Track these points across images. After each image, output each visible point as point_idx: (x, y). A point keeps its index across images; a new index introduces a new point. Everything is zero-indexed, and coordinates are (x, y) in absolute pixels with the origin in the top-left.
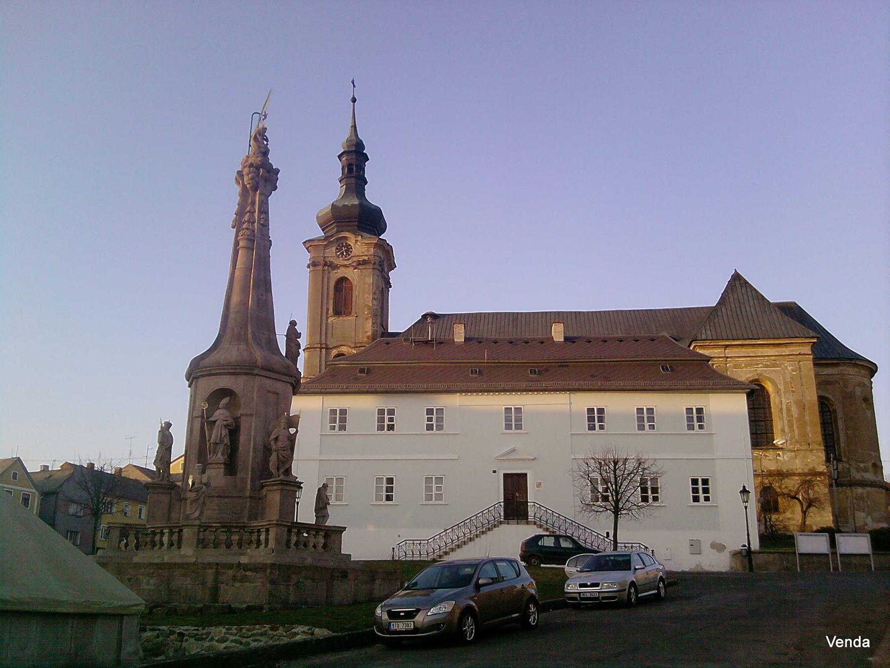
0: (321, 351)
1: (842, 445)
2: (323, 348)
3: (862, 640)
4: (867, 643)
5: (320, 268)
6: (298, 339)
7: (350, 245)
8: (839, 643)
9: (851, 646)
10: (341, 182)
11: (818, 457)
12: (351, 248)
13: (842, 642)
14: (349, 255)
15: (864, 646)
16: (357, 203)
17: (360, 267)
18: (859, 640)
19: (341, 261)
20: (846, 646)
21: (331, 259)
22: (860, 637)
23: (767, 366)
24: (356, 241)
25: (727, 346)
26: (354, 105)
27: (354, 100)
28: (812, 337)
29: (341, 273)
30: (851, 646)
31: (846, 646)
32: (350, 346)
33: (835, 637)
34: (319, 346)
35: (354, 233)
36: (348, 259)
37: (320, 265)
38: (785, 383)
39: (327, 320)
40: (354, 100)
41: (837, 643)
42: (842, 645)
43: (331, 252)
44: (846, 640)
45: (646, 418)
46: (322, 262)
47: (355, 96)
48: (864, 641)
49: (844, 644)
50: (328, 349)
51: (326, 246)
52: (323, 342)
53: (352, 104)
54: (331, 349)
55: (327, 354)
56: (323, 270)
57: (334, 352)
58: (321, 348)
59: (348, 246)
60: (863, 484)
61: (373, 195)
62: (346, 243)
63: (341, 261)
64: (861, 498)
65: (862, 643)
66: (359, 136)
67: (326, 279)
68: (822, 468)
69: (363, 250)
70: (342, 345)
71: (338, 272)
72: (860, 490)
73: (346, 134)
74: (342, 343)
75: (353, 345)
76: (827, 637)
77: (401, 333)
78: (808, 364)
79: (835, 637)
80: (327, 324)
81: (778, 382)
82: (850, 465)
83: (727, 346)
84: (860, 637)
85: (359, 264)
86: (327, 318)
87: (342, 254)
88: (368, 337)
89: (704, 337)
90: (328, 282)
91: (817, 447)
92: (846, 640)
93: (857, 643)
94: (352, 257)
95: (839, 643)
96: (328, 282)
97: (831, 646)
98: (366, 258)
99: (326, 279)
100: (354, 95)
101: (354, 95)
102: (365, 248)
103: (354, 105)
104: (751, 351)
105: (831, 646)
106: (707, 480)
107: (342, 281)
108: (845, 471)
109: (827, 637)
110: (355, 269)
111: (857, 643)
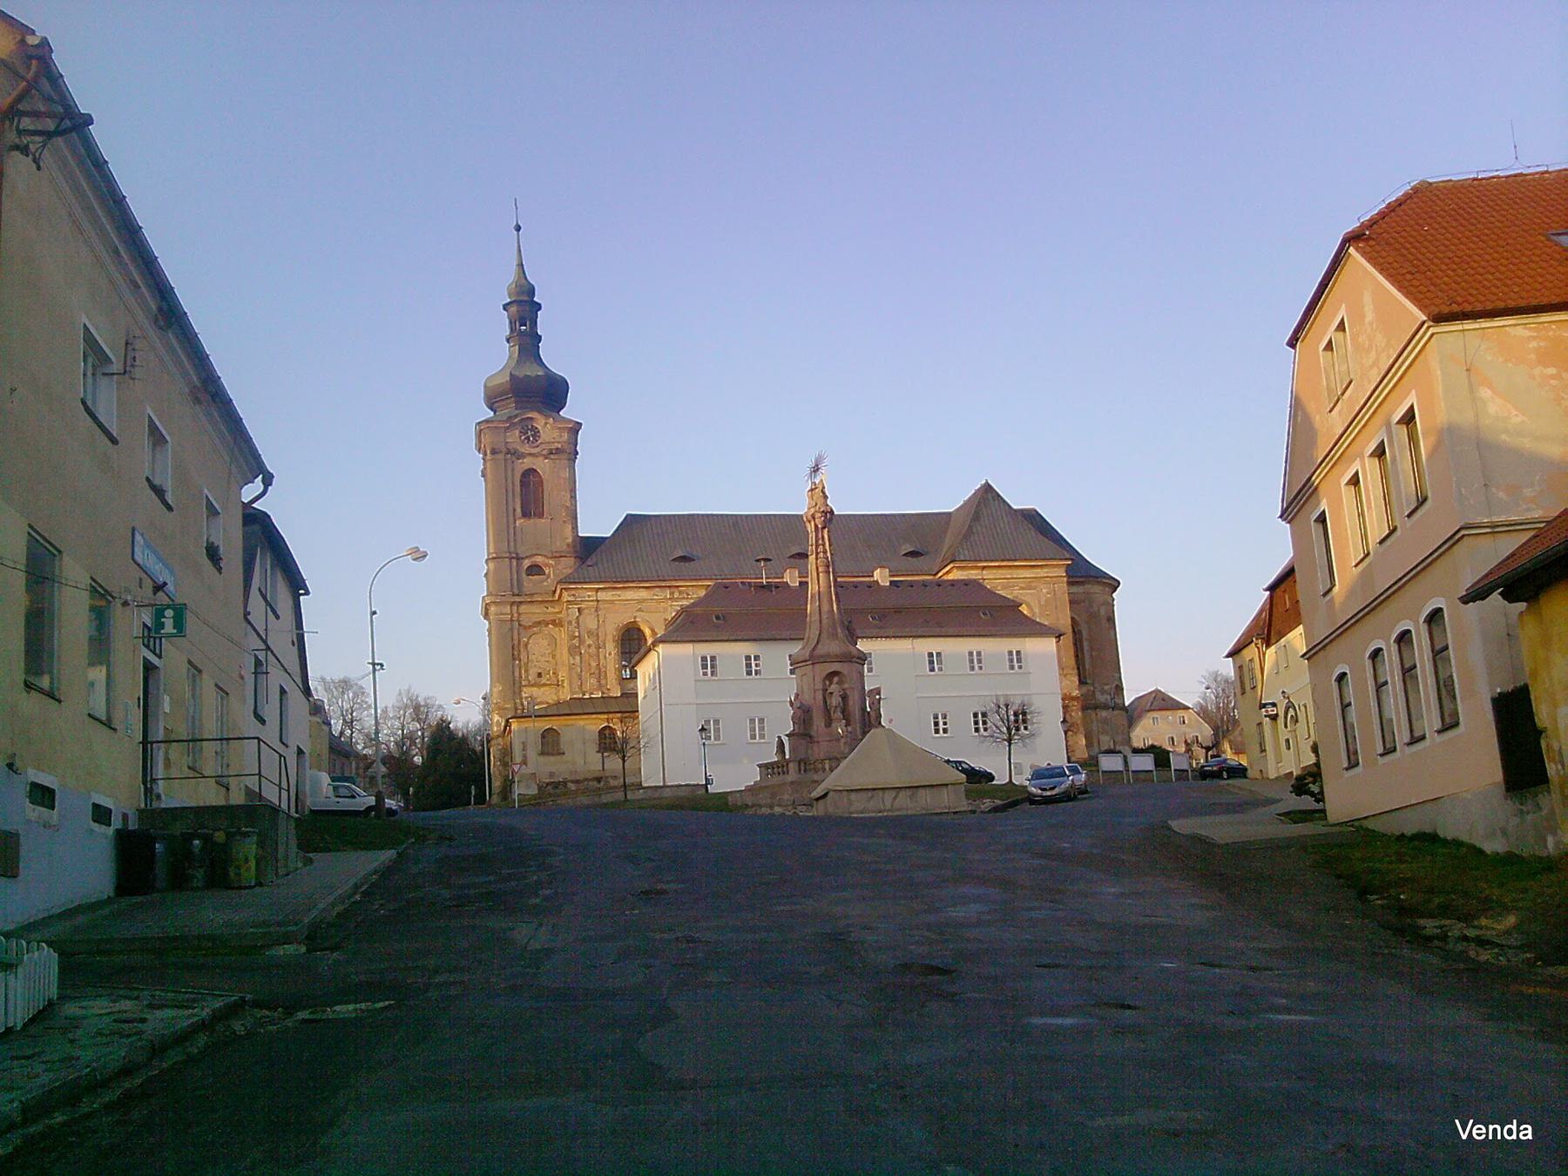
0: (511, 562)
1: (1087, 667)
2: (513, 558)
3: (1518, 1127)
4: (1528, 1133)
5: (501, 456)
6: (253, 505)
7: (537, 428)
8: (1478, 1132)
9: (1499, 1138)
10: (510, 341)
11: (1072, 682)
12: (539, 432)
13: (1484, 1131)
14: (537, 441)
15: (1522, 1137)
16: (542, 374)
17: (552, 456)
18: (1514, 1128)
19: (526, 449)
20: (1490, 1138)
21: (515, 446)
22: (1515, 1121)
23: (1022, 588)
24: (546, 423)
25: (984, 568)
26: (518, 234)
27: (518, 228)
28: (1066, 559)
29: (528, 463)
30: (1499, 1138)
31: (1490, 1138)
32: (545, 556)
33: (1471, 1121)
34: (508, 555)
35: (540, 412)
36: (537, 446)
37: (501, 452)
38: (1041, 606)
39: (515, 523)
40: (518, 228)
41: (1475, 1132)
42: (1484, 1136)
43: (514, 437)
44: (1491, 1127)
45: (975, 660)
46: (504, 450)
47: (519, 223)
48: (1522, 1128)
49: (1487, 1134)
50: (519, 559)
51: (508, 428)
52: (512, 550)
53: (516, 233)
54: (522, 558)
55: (519, 565)
56: (505, 460)
57: (527, 563)
58: (511, 558)
59: (534, 429)
60: (1105, 707)
61: (555, 357)
62: (532, 426)
63: (526, 449)
64: (1105, 721)
65: (1518, 1131)
66: (528, 278)
67: (510, 473)
68: (1076, 693)
69: (555, 436)
70: (536, 555)
71: (523, 463)
72: (1104, 713)
73: (510, 277)
74: (539, 553)
75: (550, 555)
76: (1457, 1121)
77: (606, 538)
78: (1063, 586)
79: (1471, 1121)
80: (515, 527)
81: (1032, 604)
82: (1095, 688)
83: (984, 568)
84: (1515, 1121)
85: (552, 453)
86: (515, 521)
87: (528, 438)
88: (568, 545)
89: (962, 558)
90: (513, 475)
91: (1071, 672)
92: (1491, 1127)
93: (1510, 1132)
94: (541, 443)
95: (1478, 1132)
96: (513, 475)
97: (1464, 1137)
98: (559, 446)
99: (510, 473)
100: (517, 222)
101: (517, 222)
102: (556, 434)
103: (518, 234)
104: (1007, 573)
105: (1464, 1137)
106: (986, 713)
107: (530, 473)
108: (1091, 693)
109: (1457, 1121)
110: (546, 458)
111: (1510, 1132)
